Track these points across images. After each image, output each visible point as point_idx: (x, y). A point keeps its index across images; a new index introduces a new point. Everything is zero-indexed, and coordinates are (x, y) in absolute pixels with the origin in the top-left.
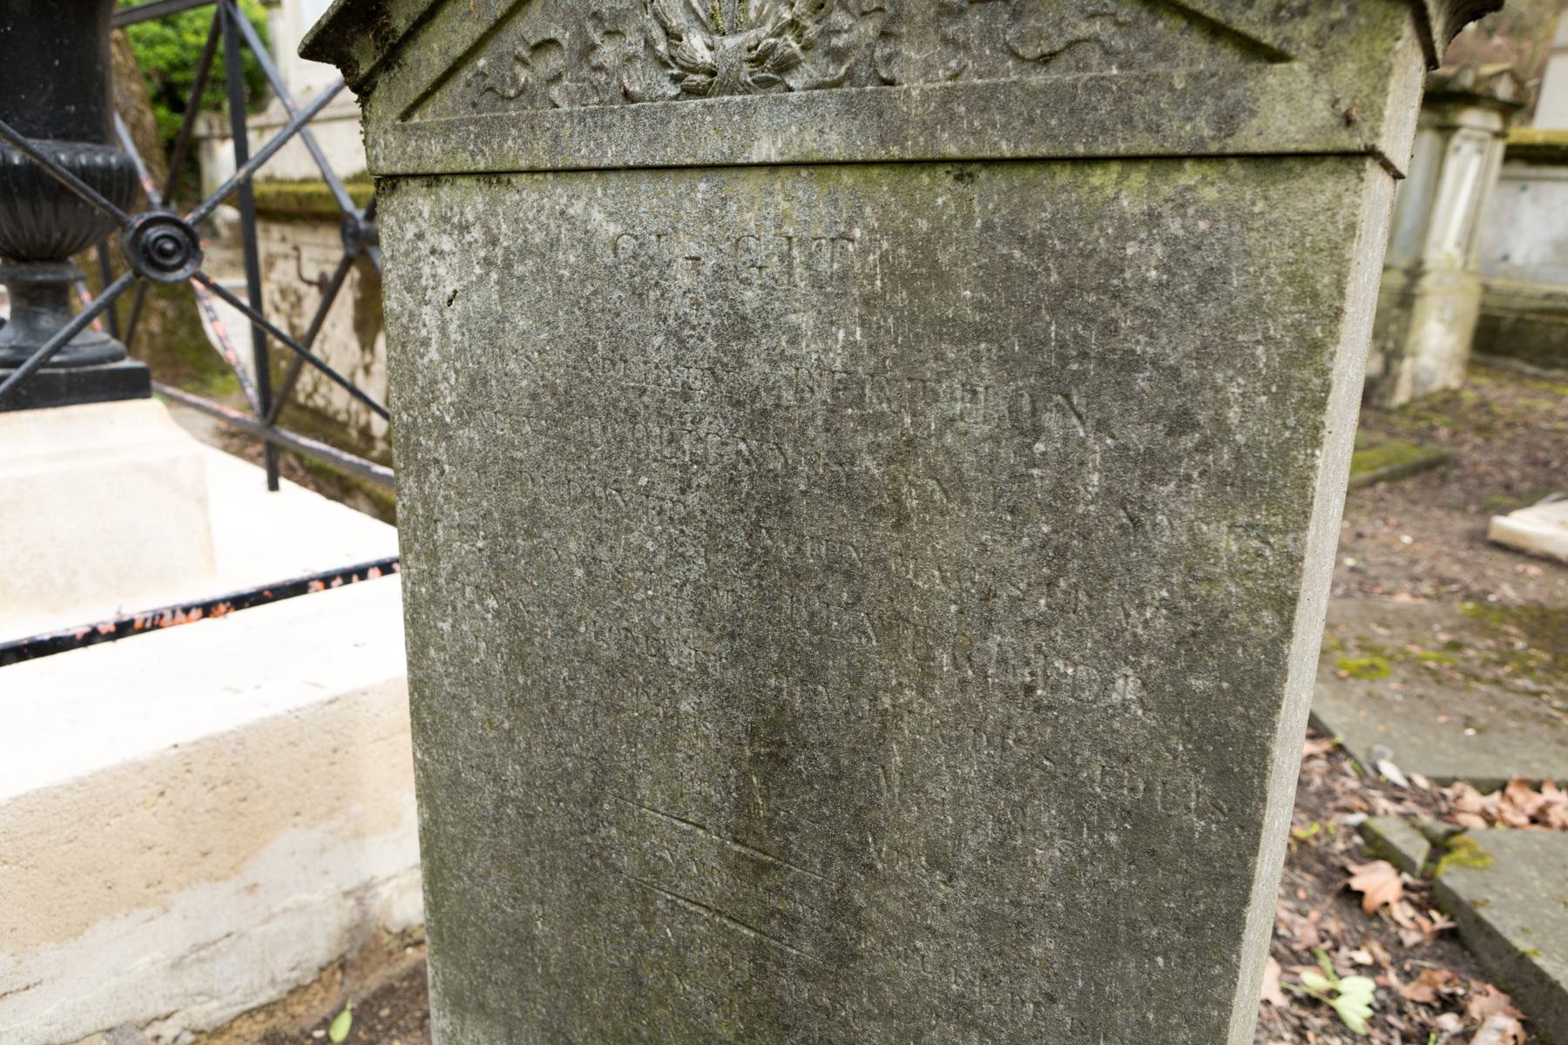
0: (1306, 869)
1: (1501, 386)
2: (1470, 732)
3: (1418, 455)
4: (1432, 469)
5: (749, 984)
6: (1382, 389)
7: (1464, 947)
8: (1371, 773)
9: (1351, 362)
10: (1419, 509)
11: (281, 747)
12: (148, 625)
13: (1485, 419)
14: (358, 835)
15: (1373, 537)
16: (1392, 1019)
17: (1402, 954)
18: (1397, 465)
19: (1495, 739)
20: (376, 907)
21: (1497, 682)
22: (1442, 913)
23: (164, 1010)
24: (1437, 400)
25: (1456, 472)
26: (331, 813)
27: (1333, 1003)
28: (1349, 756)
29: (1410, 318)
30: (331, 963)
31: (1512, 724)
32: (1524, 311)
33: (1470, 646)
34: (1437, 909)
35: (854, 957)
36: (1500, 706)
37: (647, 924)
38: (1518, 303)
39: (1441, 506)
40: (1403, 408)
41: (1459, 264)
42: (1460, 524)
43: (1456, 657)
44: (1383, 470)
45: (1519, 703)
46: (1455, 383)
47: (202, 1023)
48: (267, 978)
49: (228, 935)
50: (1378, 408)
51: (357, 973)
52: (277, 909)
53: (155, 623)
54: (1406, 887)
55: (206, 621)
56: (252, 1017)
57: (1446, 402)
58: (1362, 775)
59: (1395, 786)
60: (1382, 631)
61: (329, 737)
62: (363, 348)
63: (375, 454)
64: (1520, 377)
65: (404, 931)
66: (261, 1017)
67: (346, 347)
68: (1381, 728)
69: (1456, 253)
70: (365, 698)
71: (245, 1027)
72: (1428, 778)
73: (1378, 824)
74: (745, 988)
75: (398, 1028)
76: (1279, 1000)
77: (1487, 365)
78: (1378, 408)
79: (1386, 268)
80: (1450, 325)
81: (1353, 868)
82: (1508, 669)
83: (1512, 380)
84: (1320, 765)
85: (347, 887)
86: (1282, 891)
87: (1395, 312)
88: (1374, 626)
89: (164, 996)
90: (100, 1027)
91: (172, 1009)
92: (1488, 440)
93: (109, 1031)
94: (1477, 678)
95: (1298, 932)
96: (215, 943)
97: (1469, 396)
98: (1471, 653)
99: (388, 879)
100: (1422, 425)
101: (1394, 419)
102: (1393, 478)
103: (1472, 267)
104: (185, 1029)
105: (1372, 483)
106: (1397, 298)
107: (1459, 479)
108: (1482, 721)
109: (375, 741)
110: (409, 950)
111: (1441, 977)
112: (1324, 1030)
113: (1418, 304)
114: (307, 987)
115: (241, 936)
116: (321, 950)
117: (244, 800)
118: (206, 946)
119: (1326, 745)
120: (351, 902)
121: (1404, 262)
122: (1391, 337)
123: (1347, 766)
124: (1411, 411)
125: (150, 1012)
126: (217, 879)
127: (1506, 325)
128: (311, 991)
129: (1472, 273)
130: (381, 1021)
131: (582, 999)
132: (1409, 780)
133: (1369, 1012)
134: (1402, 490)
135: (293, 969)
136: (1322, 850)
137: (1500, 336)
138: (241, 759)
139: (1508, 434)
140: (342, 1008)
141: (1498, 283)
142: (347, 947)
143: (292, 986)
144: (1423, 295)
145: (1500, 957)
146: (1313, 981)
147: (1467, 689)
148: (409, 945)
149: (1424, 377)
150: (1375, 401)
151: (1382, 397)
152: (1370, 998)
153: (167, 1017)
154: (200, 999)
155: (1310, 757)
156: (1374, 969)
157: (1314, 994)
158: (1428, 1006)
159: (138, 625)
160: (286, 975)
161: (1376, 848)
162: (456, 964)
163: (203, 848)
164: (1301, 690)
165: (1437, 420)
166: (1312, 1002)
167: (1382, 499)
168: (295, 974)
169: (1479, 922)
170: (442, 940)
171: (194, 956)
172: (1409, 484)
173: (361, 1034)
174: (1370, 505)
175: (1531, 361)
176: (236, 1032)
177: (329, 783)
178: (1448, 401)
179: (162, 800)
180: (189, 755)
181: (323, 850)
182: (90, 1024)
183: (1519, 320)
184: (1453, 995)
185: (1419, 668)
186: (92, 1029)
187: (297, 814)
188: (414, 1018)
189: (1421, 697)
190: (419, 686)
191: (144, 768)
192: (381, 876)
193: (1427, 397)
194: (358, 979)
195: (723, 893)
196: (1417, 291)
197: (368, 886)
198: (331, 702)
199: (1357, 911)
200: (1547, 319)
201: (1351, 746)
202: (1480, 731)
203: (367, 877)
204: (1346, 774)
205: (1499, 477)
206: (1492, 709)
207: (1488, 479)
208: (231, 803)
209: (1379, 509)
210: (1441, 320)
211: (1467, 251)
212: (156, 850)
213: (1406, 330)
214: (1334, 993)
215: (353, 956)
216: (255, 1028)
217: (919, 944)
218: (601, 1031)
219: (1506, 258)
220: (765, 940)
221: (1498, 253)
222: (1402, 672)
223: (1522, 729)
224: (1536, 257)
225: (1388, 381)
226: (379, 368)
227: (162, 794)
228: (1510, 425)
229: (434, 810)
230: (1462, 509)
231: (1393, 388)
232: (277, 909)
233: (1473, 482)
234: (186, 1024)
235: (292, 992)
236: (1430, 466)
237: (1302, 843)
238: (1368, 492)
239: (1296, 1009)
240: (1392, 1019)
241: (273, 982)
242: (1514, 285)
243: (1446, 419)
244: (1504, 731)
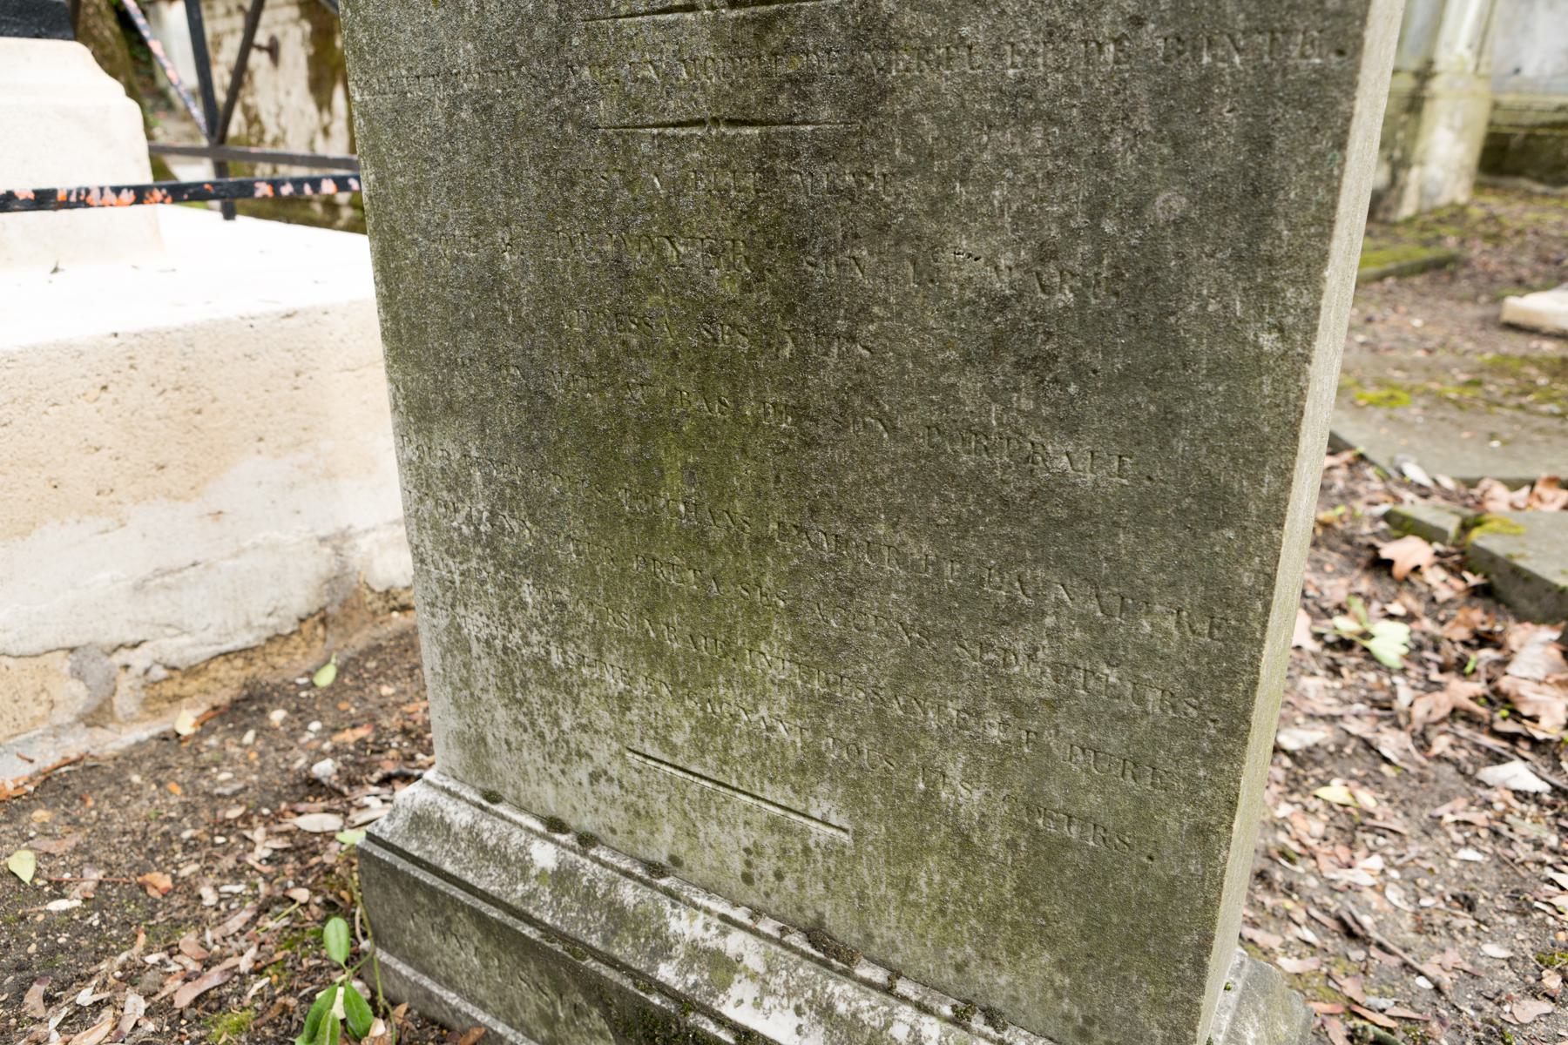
0: (1331, 548)
1: (1509, 204)
2: (1495, 444)
3: (1426, 254)
4: (1441, 268)
5: (754, 207)
6: (1387, 202)
7: (1498, 601)
8: (1395, 475)
9: (1362, 169)
10: (1429, 300)
11: (236, 359)
12: (73, 199)
13: (1493, 229)
14: (330, 475)
15: (1383, 321)
16: (1428, 654)
17: (1435, 607)
18: (1405, 262)
19: (1522, 449)
20: (355, 560)
21: (1521, 407)
22: (1475, 574)
23: (131, 638)
24: (1444, 214)
25: (1465, 271)
26: (297, 445)
27: (1367, 644)
28: (1372, 464)
29: (1418, 124)
30: (311, 615)
31: (1537, 437)
32: (1534, 126)
33: (1490, 383)
34: (1470, 570)
35: (883, 94)
36: (1524, 426)
37: (629, 185)
38: (1528, 119)
39: (1451, 298)
40: (1409, 221)
41: (1471, 68)
42: (1471, 312)
43: (1478, 391)
44: (1391, 266)
45: (1544, 422)
46: (1462, 198)
47: (174, 660)
48: (242, 620)
49: (194, 565)
50: (1384, 222)
51: (341, 630)
52: (247, 544)
53: (80, 200)
54: (1437, 554)
55: (139, 207)
56: (228, 660)
57: (1453, 216)
58: (1385, 478)
59: (1420, 486)
60: (1398, 374)
61: (289, 355)
62: (320, 108)
63: (341, 223)
64: (1529, 195)
65: (387, 592)
66: (239, 663)
67: (302, 113)
68: (1404, 442)
69: (1468, 55)
70: (326, 317)
71: (221, 670)
72: (1454, 479)
73: (1405, 509)
74: (749, 214)
75: (386, 676)
76: (1311, 646)
77: (1494, 186)
78: (1384, 222)
79: (1396, 72)
80: (1460, 132)
81: (1379, 544)
82: (1531, 398)
83: (1520, 198)
84: (1340, 475)
85: (322, 533)
86: (1308, 567)
87: (1403, 118)
88: (1390, 372)
89: (129, 621)
90: (61, 644)
91: (140, 638)
92: (1497, 246)
93: (72, 650)
94: (1500, 405)
95: (1327, 592)
96: (180, 570)
97: (1476, 212)
98: (1492, 388)
99: (367, 531)
100: (1429, 235)
101: (1399, 231)
102: (1402, 273)
103: (1483, 70)
104: (156, 662)
105: (1381, 278)
106: (1406, 103)
107: (1468, 277)
108: (1508, 436)
109: (342, 370)
110: (395, 614)
111: (1477, 616)
112: (1358, 667)
113: (1427, 106)
114: (287, 638)
115: (208, 567)
116: (300, 599)
117: (199, 412)
118: (171, 572)
119: (1347, 456)
120: (328, 550)
121: (1414, 64)
122: (1398, 158)
123: (1370, 472)
124: (1417, 223)
125: (116, 637)
126: (177, 499)
127: (1514, 143)
128: (292, 644)
129: (1485, 77)
130: (367, 670)
131: (559, 333)
132: (1435, 481)
133: (1405, 650)
134: (1411, 286)
135: (270, 615)
136: (1349, 532)
137: (1506, 156)
138: (192, 364)
139: (1517, 241)
140: (327, 662)
141: (1508, 99)
142: (327, 599)
143: (270, 633)
144: (1433, 98)
145: (1539, 599)
146: (1346, 626)
147: (1489, 413)
148: (393, 609)
149: (1431, 188)
150: (1380, 216)
151: (1388, 210)
152: (1406, 638)
153: (135, 646)
154: (170, 631)
155: (1330, 468)
156: (1409, 618)
157: (1347, 637)
158: (1465, 643)
159: (61, 196)
160: (263, 620)
161: (1401, 526)
162: (419, 365)
163: (158, 460)
164: (1320, 414)
165: (1443, 230)
166: (1345, 645)
167: (1390, 292)
168: (272, 621)
169: (1516, 572)
170: (401, 340)
171: (158, 581)
172: (1417, 280)
173: (347, 681)
174: (1378, 298)
175: (1540, 180)
176: (213, 675)
177: (293, 410)
178: (1457, 214)
179: (104, 395)
180: (132, 348)
181: (292, 486)
182: (49, 638)
183: (1528, 136)
184: (1490, 633)
185: (1441, 400)
186: (52, 646)
187: (261, 439)
188: (402, 670)
189: (1443, 419)
190: (388, 300)
191: (81, 354)
192: (360, 527)
193: (1432, 211)
194: (342, 636)
195: (718, 89)
196: (1426, 94)
197: (345, 535)
198: (288, 316)
199: (1387, 580)
200: (1558, 133)
201: (1371, 455)
202: (1505, 443)
203: (344, 525)
204: (1368, 480)
205: (1510, 275)
206: (1516, 427)
207: (1499, 277)
208: (185, 413)
209: (1388, 299)
210: (1451, 127)
211: (1480, 54)
212: (103, 451)
213: (1414, 136)
214: (1366, 635)
215: (334, 610)
216: (234, 673)
217: (965, 30)
218: (584, 365)
219: (1517, 71)
220: (773, 129)
221: (1510, 67)
222: (1422, 402)
223: (1548, 441)
224: (1549, 68)
225: (1394, 193)
226: (339, 127)
227: (105, 388)
228: (1519, 232)
229: (395, 318)
230: (1474, 300)
231: (1399, 201)
232: (247, 544)
233: (1482, 280)
234: (157, 657)
235: (269, 640)
236: (1438, 266)
237: (1326, 525)
238: (1376, 286)
239: (1328, 653)
240: (1428, 654)
241: (249, 625)
242: (1525, 99)
243: (1453, 229)
244: (1530, 443)
